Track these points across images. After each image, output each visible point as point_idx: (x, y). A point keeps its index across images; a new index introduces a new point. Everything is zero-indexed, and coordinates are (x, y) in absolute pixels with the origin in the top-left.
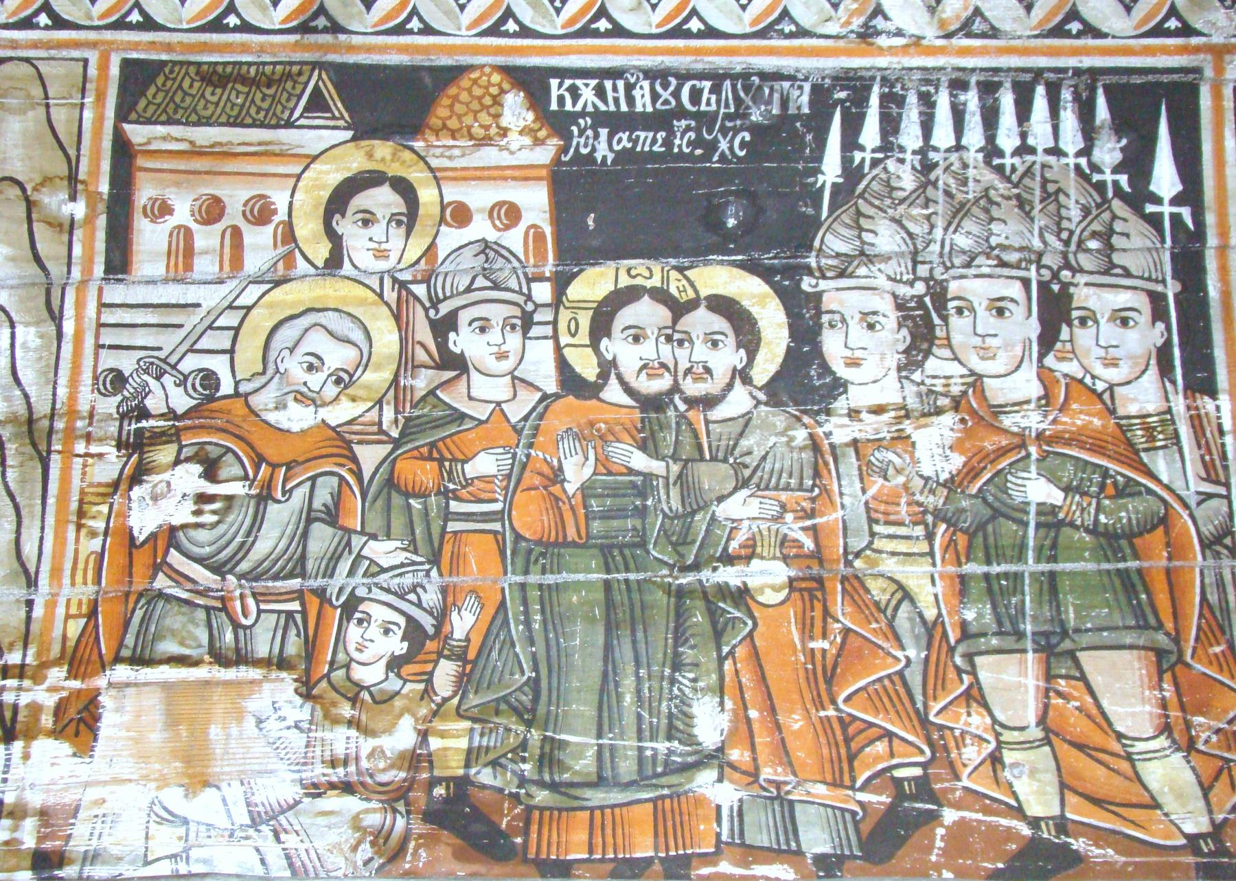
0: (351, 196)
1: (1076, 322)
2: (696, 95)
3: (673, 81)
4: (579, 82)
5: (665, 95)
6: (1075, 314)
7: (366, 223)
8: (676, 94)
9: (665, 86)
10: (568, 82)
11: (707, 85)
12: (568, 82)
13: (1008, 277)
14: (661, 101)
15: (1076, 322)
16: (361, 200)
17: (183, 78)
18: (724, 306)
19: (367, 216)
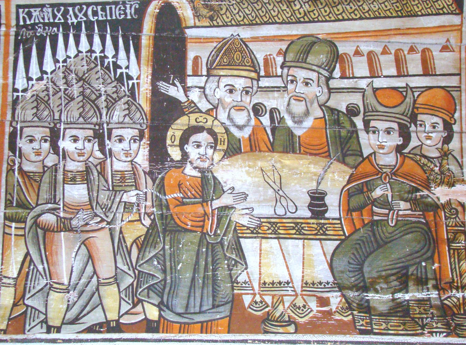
0: (189, 136)
1: (418, 125)
2: (95, 13)
3: (62, 8)
4: (32, 10)
5: (59, 15)
6: (418, 123)
7: (31, 141)
8: (86, 15)
9: (59, 11)
10: (26, 10)
11: (99, 8)
12: (26, 10)
13: (434, 107)
14: (57, 18)
15: (418, 125)
16: (194, 138)
17: (259, 13)
18: (184, 140)
19: (77, 138)
